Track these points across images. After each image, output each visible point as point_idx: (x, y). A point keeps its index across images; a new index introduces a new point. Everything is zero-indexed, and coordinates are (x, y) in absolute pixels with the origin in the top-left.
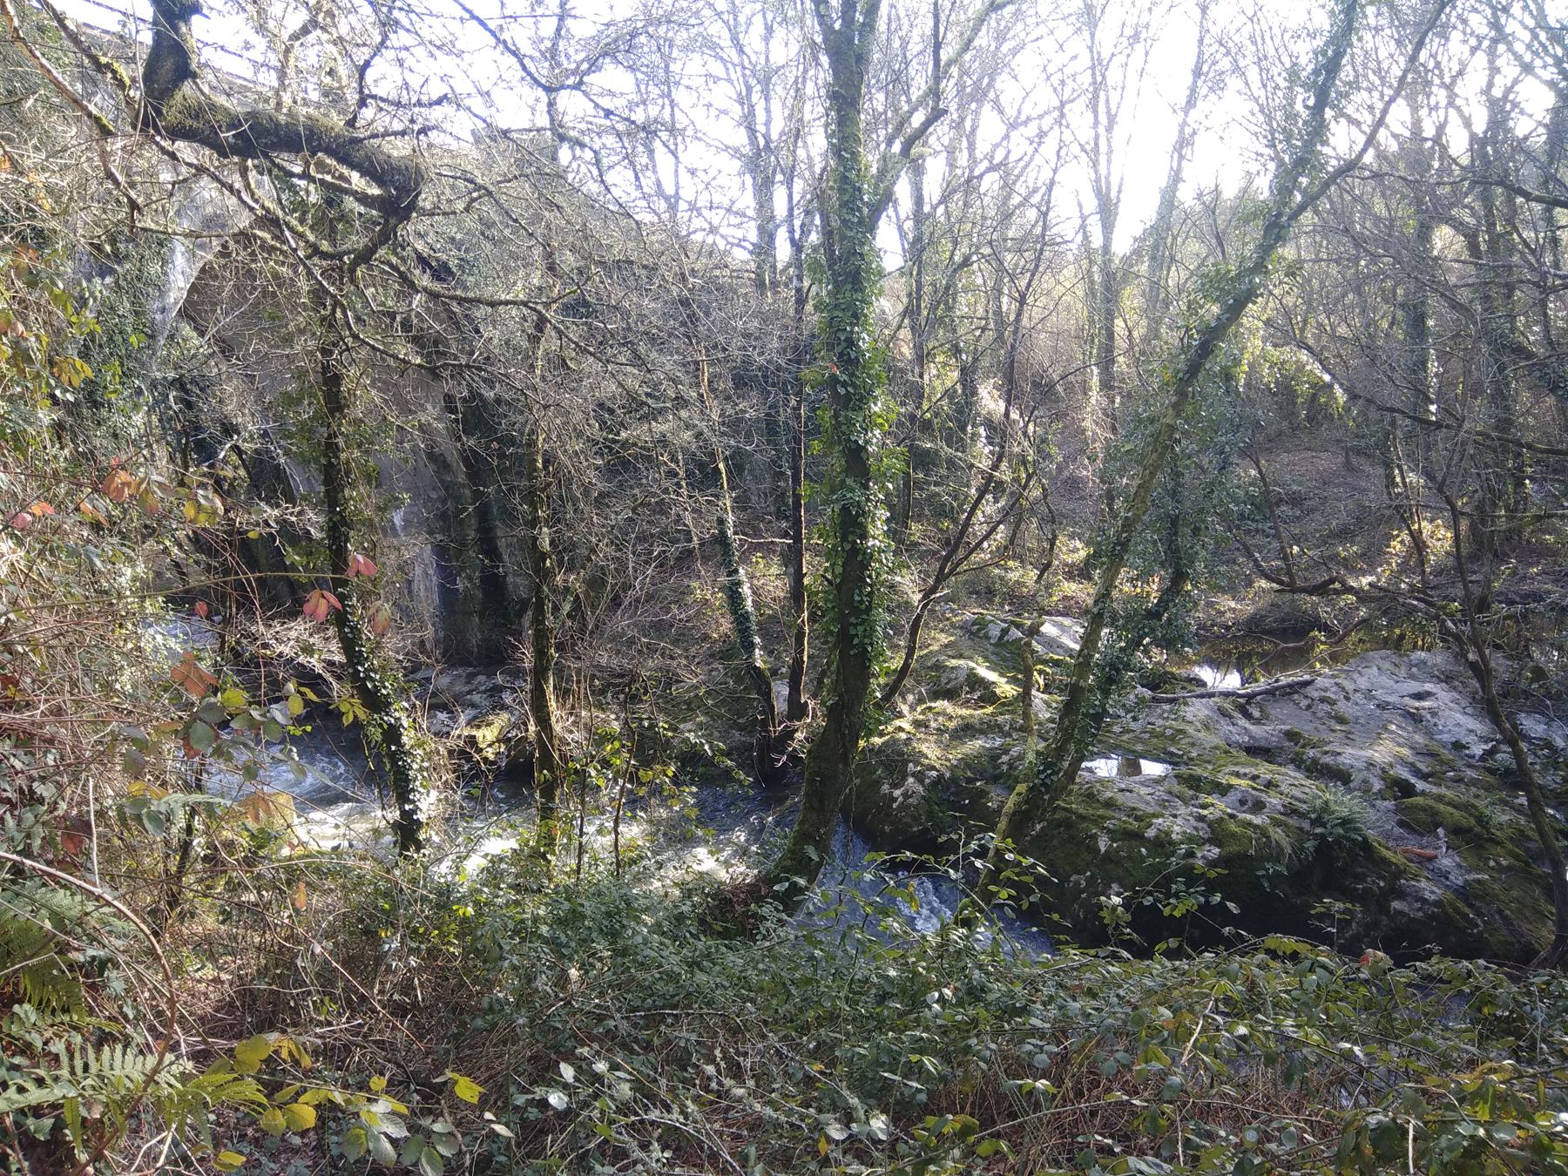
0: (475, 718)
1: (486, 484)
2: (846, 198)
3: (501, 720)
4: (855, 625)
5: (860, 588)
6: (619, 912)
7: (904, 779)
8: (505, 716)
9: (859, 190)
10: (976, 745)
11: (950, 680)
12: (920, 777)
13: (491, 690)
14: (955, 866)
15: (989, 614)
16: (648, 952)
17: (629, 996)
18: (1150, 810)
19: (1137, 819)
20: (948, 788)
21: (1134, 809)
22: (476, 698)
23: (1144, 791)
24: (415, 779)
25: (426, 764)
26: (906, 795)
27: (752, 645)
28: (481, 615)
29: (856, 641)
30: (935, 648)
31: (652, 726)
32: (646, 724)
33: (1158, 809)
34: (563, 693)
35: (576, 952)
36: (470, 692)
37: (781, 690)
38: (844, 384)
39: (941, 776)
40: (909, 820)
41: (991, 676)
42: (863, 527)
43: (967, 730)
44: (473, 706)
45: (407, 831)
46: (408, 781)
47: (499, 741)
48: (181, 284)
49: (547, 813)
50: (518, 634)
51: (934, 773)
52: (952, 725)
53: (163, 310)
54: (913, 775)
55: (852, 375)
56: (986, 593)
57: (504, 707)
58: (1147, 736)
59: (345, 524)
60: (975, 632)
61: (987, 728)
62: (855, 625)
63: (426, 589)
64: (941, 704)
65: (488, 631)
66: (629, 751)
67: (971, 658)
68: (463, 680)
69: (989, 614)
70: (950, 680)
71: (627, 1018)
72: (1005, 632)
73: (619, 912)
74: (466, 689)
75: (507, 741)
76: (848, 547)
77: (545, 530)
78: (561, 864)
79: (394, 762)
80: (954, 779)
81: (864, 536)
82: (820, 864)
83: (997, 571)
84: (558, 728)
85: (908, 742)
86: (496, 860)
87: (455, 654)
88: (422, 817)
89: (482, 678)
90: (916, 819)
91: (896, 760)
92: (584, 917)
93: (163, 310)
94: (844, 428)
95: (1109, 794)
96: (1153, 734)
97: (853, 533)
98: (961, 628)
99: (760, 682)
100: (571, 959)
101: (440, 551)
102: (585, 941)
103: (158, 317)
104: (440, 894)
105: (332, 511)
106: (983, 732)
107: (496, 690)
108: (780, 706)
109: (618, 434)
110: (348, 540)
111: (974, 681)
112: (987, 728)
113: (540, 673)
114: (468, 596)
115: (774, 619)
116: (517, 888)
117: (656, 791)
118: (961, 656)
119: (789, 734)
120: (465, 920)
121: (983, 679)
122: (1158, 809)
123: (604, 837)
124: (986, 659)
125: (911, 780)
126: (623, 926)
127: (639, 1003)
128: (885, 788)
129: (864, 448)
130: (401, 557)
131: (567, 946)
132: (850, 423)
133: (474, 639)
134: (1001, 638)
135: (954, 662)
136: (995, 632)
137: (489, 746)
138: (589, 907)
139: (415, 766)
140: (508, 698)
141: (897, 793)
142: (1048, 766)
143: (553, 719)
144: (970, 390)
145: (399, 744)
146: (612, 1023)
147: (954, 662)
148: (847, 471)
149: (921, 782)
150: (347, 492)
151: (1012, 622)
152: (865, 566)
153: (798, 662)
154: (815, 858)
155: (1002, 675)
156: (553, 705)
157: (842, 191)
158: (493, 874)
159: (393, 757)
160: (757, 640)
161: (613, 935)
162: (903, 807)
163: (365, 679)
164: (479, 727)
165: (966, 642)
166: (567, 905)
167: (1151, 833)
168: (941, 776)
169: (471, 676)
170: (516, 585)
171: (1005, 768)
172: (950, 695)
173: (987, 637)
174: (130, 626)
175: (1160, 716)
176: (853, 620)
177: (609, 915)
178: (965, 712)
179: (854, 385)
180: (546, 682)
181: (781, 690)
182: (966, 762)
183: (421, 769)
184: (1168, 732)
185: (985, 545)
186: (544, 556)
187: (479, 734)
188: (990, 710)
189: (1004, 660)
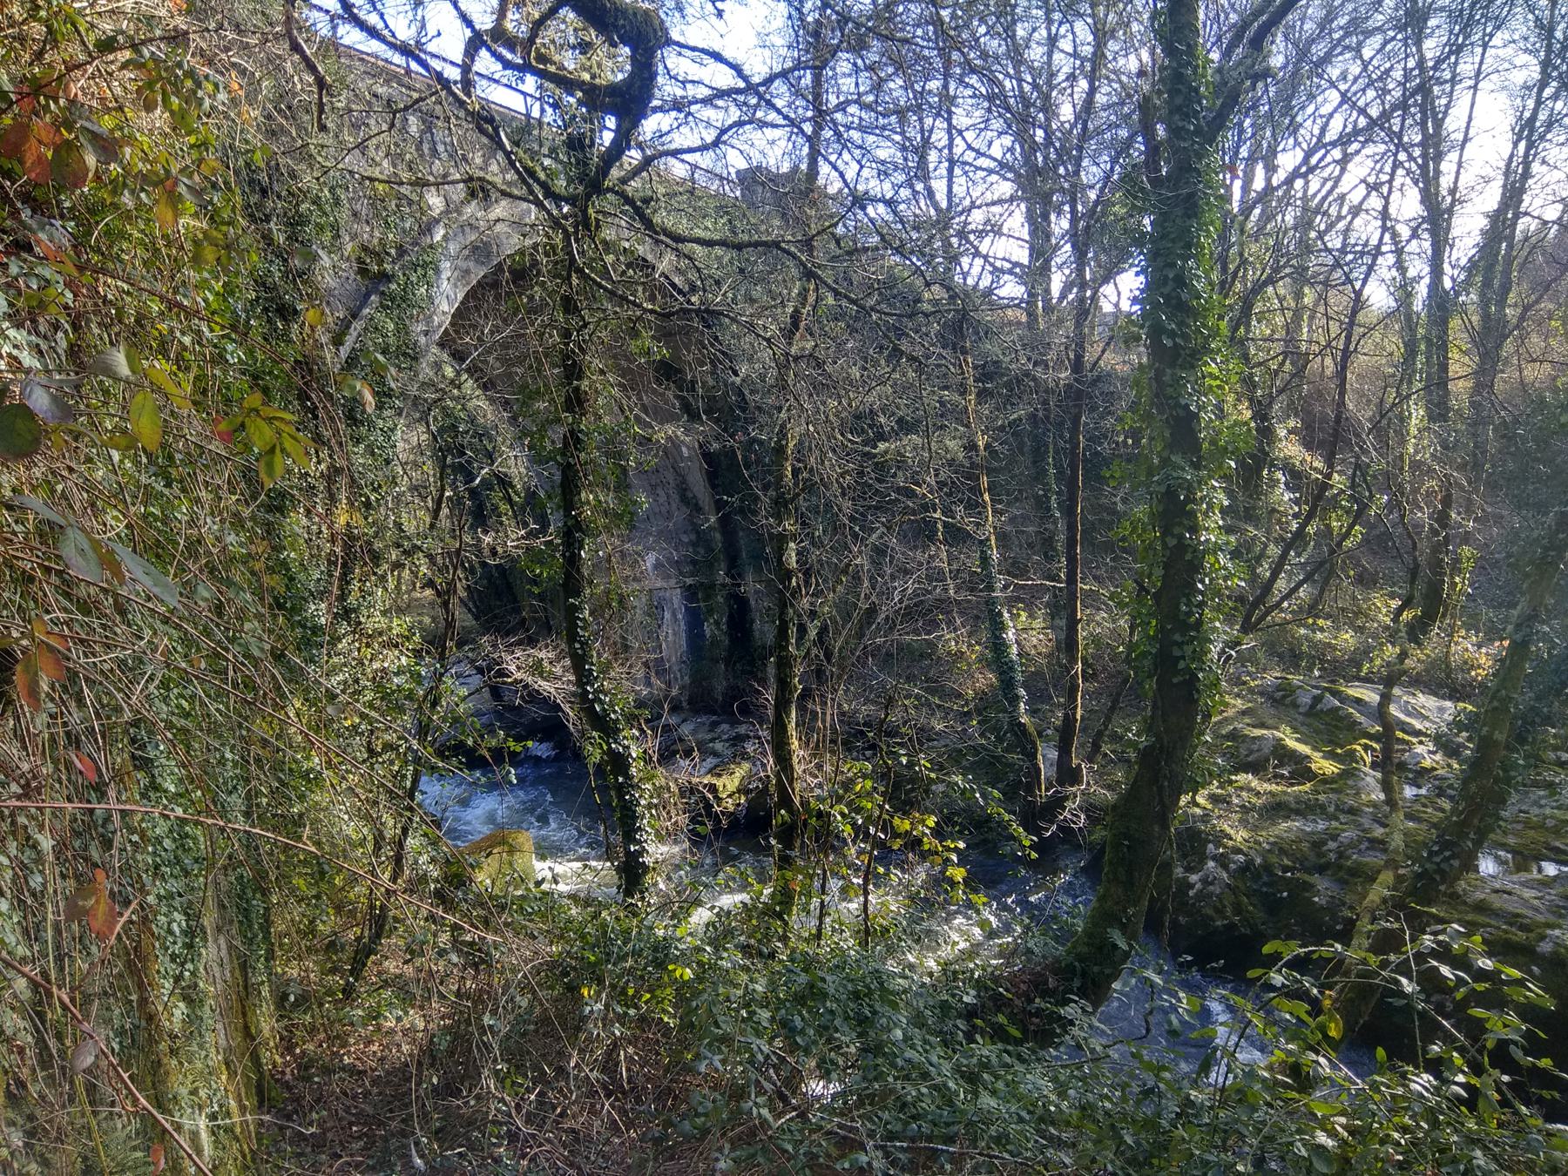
0: (716, 766)
1: (734, 502)
2: (1179, 101)
3: (741, 771)
4: (1180, 645)
5: (1187, 596)
6: (870, 993)
7: (1203, 859)
8: (746, 766)
9: (1196, 90)
10: (1287, 827)
11: (1251, 752)
12: (1222, 861)
13: (735, 738)
14: (1404, 969)
15: (1296, 679)
16: (910, 1054)
17: (886, 1116)
18: (1540, 918)
19: (1523, 928)
20: (1259, 876)
21: (1518, 915)
22: (718, 746)
23: (1528, 894)
24: (643, 817)
25: (655, 801)
26: (1205, 882)
27: (1017, 698)
28: (727, 662)
29: (1182, 665)
30: (1230, 713)
31: (911, 765)
32: (904, 760)
33: (1552, 919)
34: (807, 727)
35: (815, 1043)
36: (713, 740)
37: (1047, 756)
38: (1172, 335)
39: (1250, 863)
40: (1210, 912)
41: (1304, 749)
42: (1192, 515)
43: (1277, 809)
44: (715, 754)
45: (632, 873)
46: (634, 818)
47: (739, 791)
48: (446, 309)
49: (785, 862)
50: (763, 682)
51: (1241, 858)
52: (1259, 802)
53: (426, 333)
54: (1214, 858)
55: (1181, 324)
56: (1292, 658)
57: (745, 756)
58: (1519, 827)
59: (580, 530)
60: (1281, 700)
61: (1304, 809)
62: (1180, 645)
63: (675, 634)
64: (1242, 778)
65: (731, 678)
66: (883, 794)
67: (1277, 728)
68: (707, 728)
69: (1296, 679)
70: (1251, 752)
71: (883, 1148)
72: (1317, 699)
73: (870, 993)
74: (709, 736)
75: (746, 792)
76: (1172, 542)
77: (792, 545)
78: (800, 922)
79: (621, 797)
80: (1267, 867)
81: (1195, 529)
82: (1127, 955)
83: (1302, 631)
84: (799, 769)
85: (1206, 818)
86: (724, 914)
87: (698, 702)
88: (647, 860)
89: (725, 727)
90: (1220, 911)
91: (1195, 842)
92: (824, 995)
93: (426, 333)
94: (1169, 391)
95: (1479, 895)
96: (1528, 824)
97: (1180, 524)
98: (1262, 694)
99: (1024, 742)
100: (807, 1052)
101: (690, 593)
102: (826, 1028)
103: (422, 340)
104: (655, 950)
105: (567, 515)
106: (1298, 812)
107: (738, 740)
108: (1046, 770)
109: (875, 447)
110: (581, 547)
111: (1283, 754)
112: (1304, 809)
113: (782, 705)
114: (715, 643)
115: (1038, 674)
116: (745, 949)
117: (914, 843)
118: (1263, 726)
119: (1058, 802)
120: (683, 985)
121: (1295, 751)
122: (1552, 919)
123: (843, 908)
124: (1295, 730)
125: (1211, 864)
126: (875, 1013)
127: (899, 1127)
128: (1179, 871)
129: (1196, 416)
130: (639, 573)
131: (802, 1032)
132: (1177, 382)
133: (720, 687)
134: (1312, 706)
135: (1258, 732)
136: (1305, 700)
137: (730, 796)
138: (831, 983)
139: (643, 802)
140: (750, 748)
141: (1194, 878)
142: (1445, 845)
143: (795, 760)
144: (1266, 433)
145: (628, 777)
146: (864, 1159)
147: (1258, 732)
148: (1172, 446)
149: (1225, 867)
150: (583, 495)
151: (1326, 689)
152: (1195, 567)
153: (1069, 721)
154: (1123, 945)
155: (1315, 749)
156: (795, 744)
157: (1173, 93)
158: (720, 934)
159: (621, 790)
160: (1022, 692)
161: (863, 1023)
162: (1201, 896)
163: (593, 701)
164: (720, 775)
165: (1267, 712)
166: (803, 978)
167: (1545, 947)
168: (1250, 863)
169: (714, 725)
170: (762, 632)
171: (1332, 856)
172: (1256, 768)
173: (1295, 705)
174: (376, 646)
175: (1536, 803)
176: (1177, 637)
177: (856, 996)
178: (1274, 788)
179: (1186, 337)
180: (788, 716)
181: (1047, 756)
182: (1280, 848)
183: (650, 806)
184: (1550, 823)
185: (1285, 604)
186: (789, 574)
187: (719, 783)
188: (1307, 787)
189: (1317, 732)
